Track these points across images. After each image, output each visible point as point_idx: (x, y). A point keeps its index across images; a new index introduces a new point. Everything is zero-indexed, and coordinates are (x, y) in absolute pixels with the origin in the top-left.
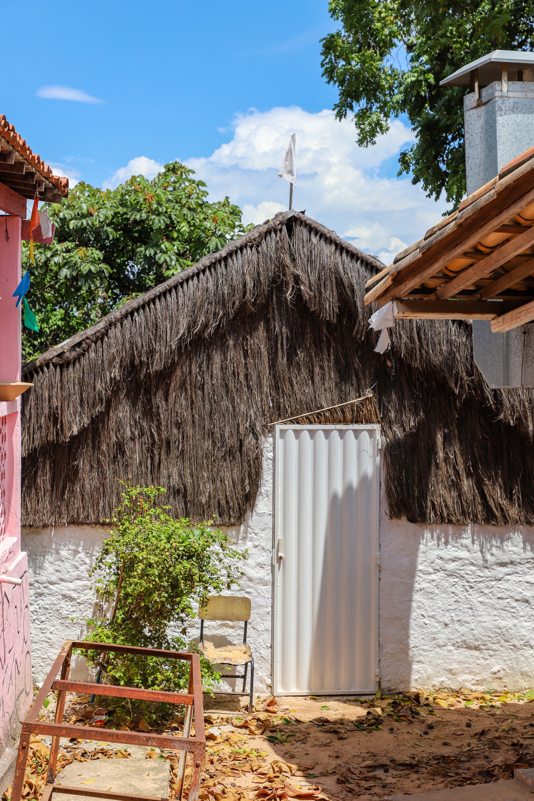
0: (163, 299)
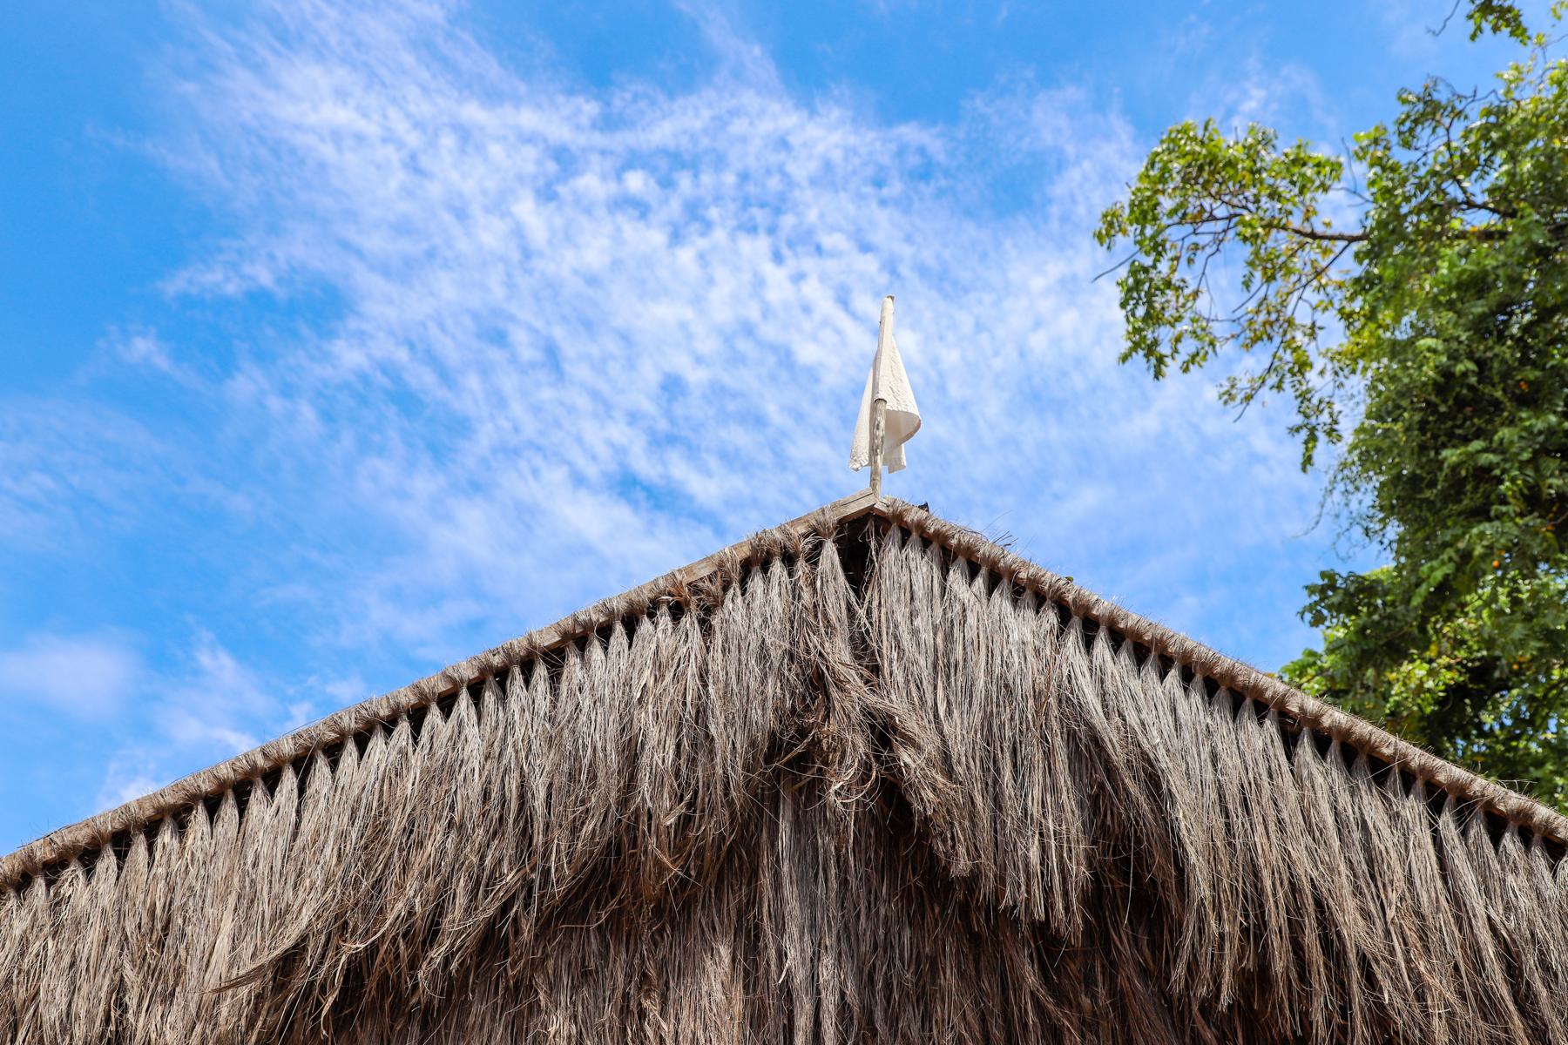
0: (229, 810)
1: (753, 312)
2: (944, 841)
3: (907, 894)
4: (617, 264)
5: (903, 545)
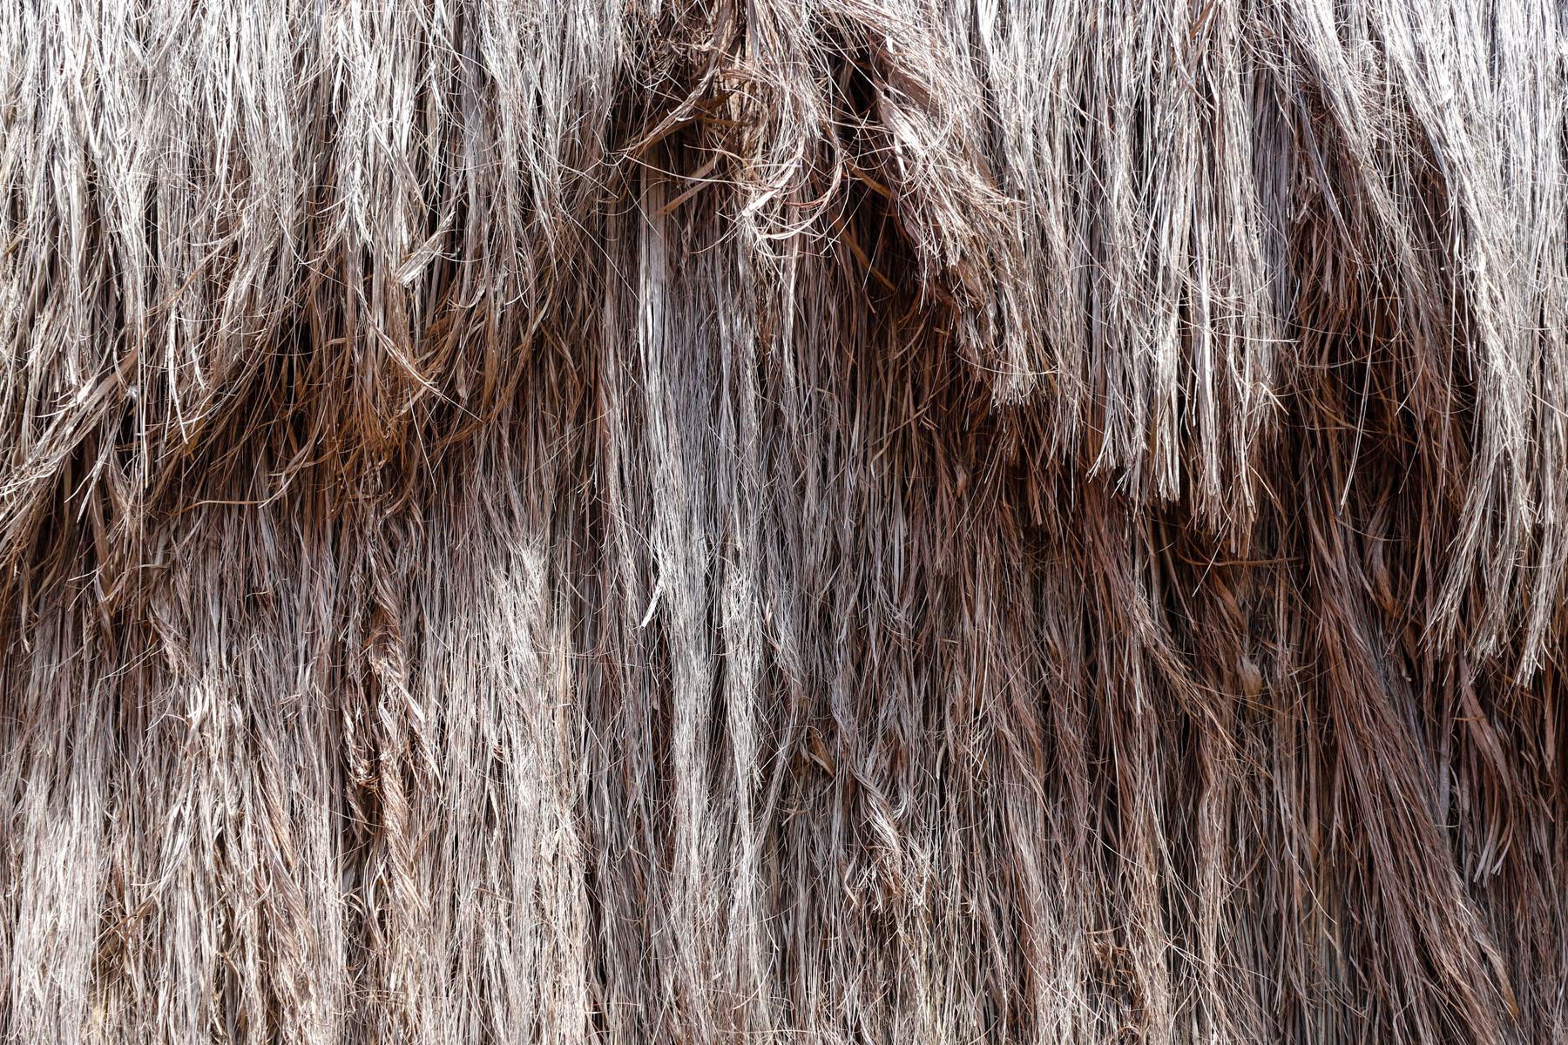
2: (981, 326)
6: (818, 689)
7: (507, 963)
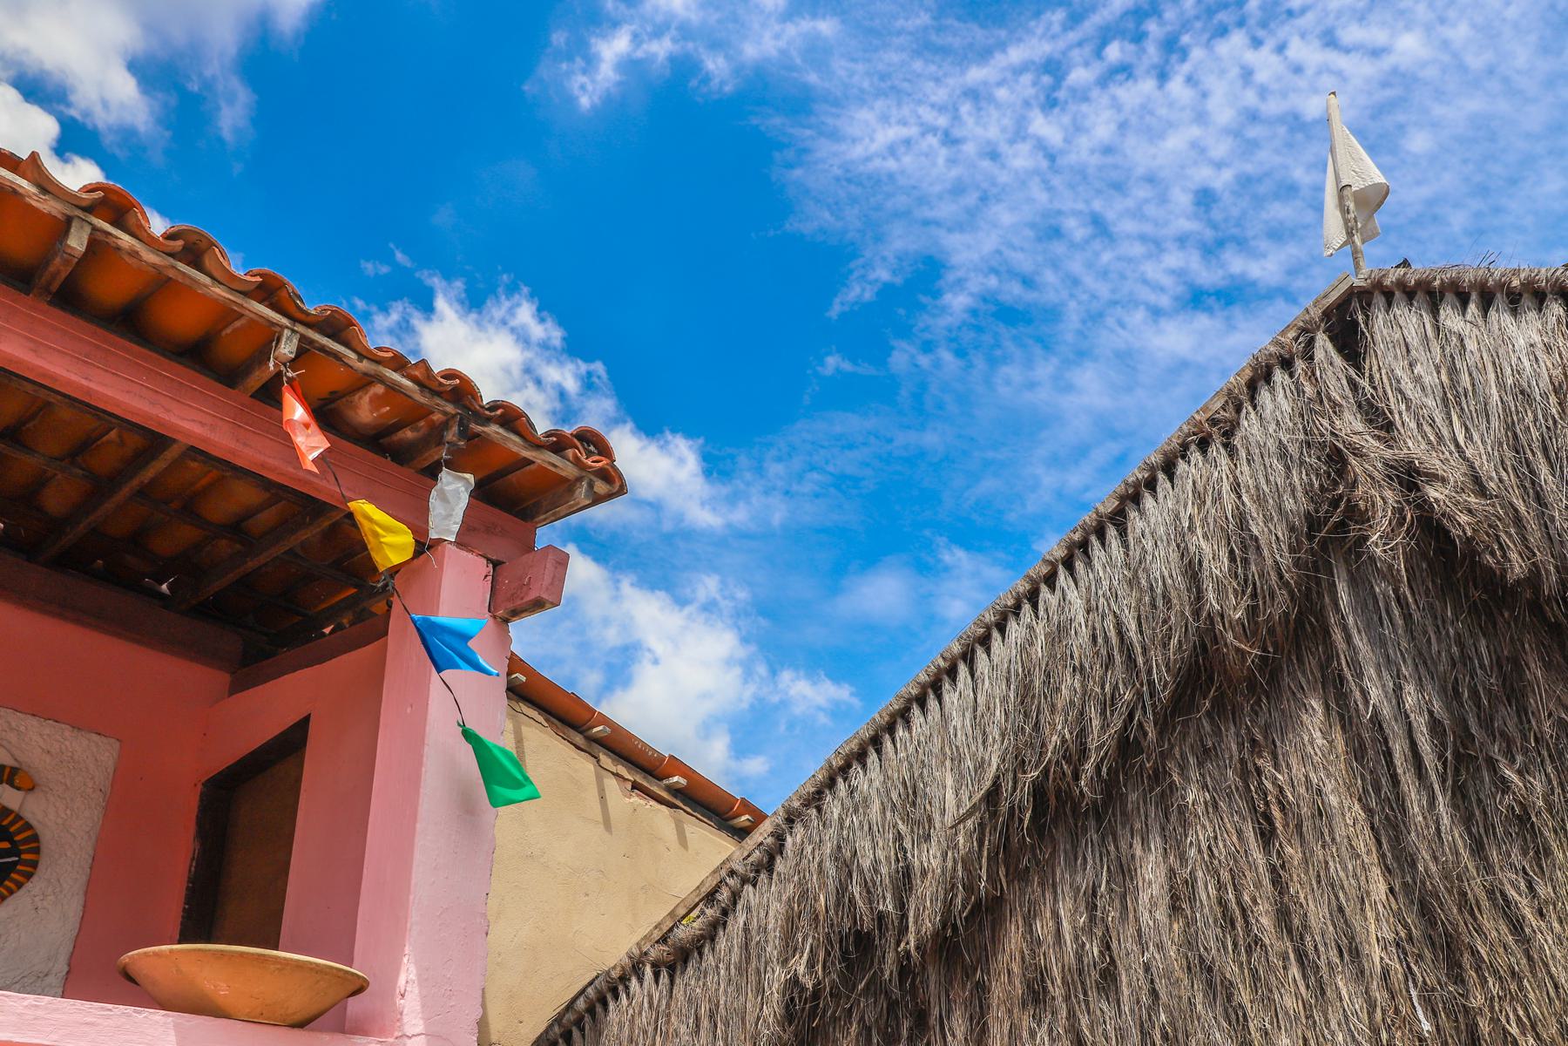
0: (932, 703)
1: (1250, 98)
2: (1493, 554)
3: (1474, 609)
4: (1123, 126)
5: (1389, 305)
6: (1462, 723)
7: (1342, 874)
